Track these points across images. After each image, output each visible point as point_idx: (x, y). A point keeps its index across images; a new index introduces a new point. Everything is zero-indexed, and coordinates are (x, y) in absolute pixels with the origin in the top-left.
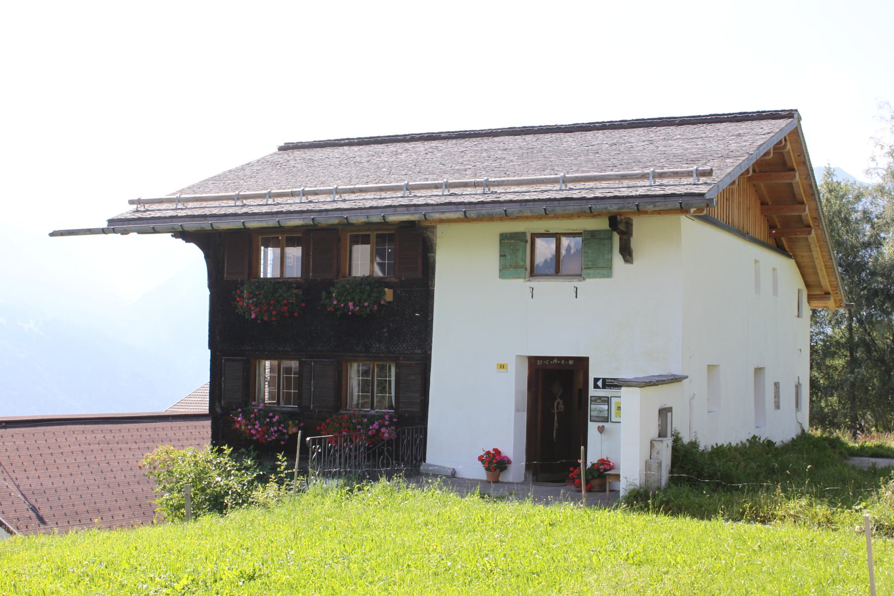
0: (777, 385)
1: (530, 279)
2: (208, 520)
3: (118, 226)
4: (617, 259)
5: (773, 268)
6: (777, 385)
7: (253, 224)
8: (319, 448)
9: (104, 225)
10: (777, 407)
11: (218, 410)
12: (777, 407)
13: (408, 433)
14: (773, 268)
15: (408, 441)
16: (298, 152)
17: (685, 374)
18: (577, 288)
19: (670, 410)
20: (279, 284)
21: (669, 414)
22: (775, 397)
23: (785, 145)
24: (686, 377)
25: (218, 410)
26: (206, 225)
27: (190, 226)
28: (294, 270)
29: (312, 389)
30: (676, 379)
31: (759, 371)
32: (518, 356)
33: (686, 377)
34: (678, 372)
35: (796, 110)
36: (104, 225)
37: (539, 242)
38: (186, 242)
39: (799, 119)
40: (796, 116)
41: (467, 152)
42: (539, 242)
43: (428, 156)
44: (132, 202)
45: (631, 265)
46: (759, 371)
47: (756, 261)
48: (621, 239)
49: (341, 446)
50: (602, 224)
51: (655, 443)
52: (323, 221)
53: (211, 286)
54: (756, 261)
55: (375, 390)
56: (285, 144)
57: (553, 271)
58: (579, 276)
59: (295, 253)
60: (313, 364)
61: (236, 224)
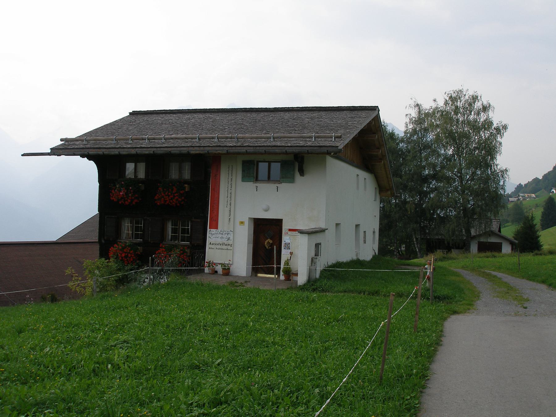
0: (365, 232)
1: (256, 182)
2: (46, 307)
3: (56, 151)
4: (297, 174)
5: (357, 175)
6: (365, 232)
7: (124, 152)
8: (165, 259)
9: (49, 151)
10: (365, 242)
11: (103, 241)
12: (365, 242)
13: (197, 253)
14: (357, 175)
15: (197, 257)
16: (140, 116)
17: (327, 228)
18: (278, 187)
19: (320, 244)
20: (135, 181)
21: (320, 246)
22: (364, 238)
23: (372, 122)
24: (327, 229)
25: (103, 241)
26: (100, 152)
27: (92, 152)
28: (142, 175)
29: (150, 232)
30: (323, 231)
31: (357, 226)
32: (249, 218)
33: (327, 229)
34: (323, 226)
35: (378, 106)
36: (49, 151)
37: (260, 164)
38: (89, 160)
39: (379, 111)
40: (377, 109)
41: (224, 120)
42: (260, 164)
43: (206, 121)
44: (62, 140)
45: (303, 177)
46: (357, 226)
47: (358, 175)
48: (299, 165)
49: (199, 255)
50: (291, 157)
51: (314, 259)
52: (160, 151)
53: (100, 181)
54: (358, 175)
55: (180, 233)
56: (133, 111)
57: (266, 178)
58: (279, 182)
59: (142, 167)
60: (150, 220)
61: (116, 152)
